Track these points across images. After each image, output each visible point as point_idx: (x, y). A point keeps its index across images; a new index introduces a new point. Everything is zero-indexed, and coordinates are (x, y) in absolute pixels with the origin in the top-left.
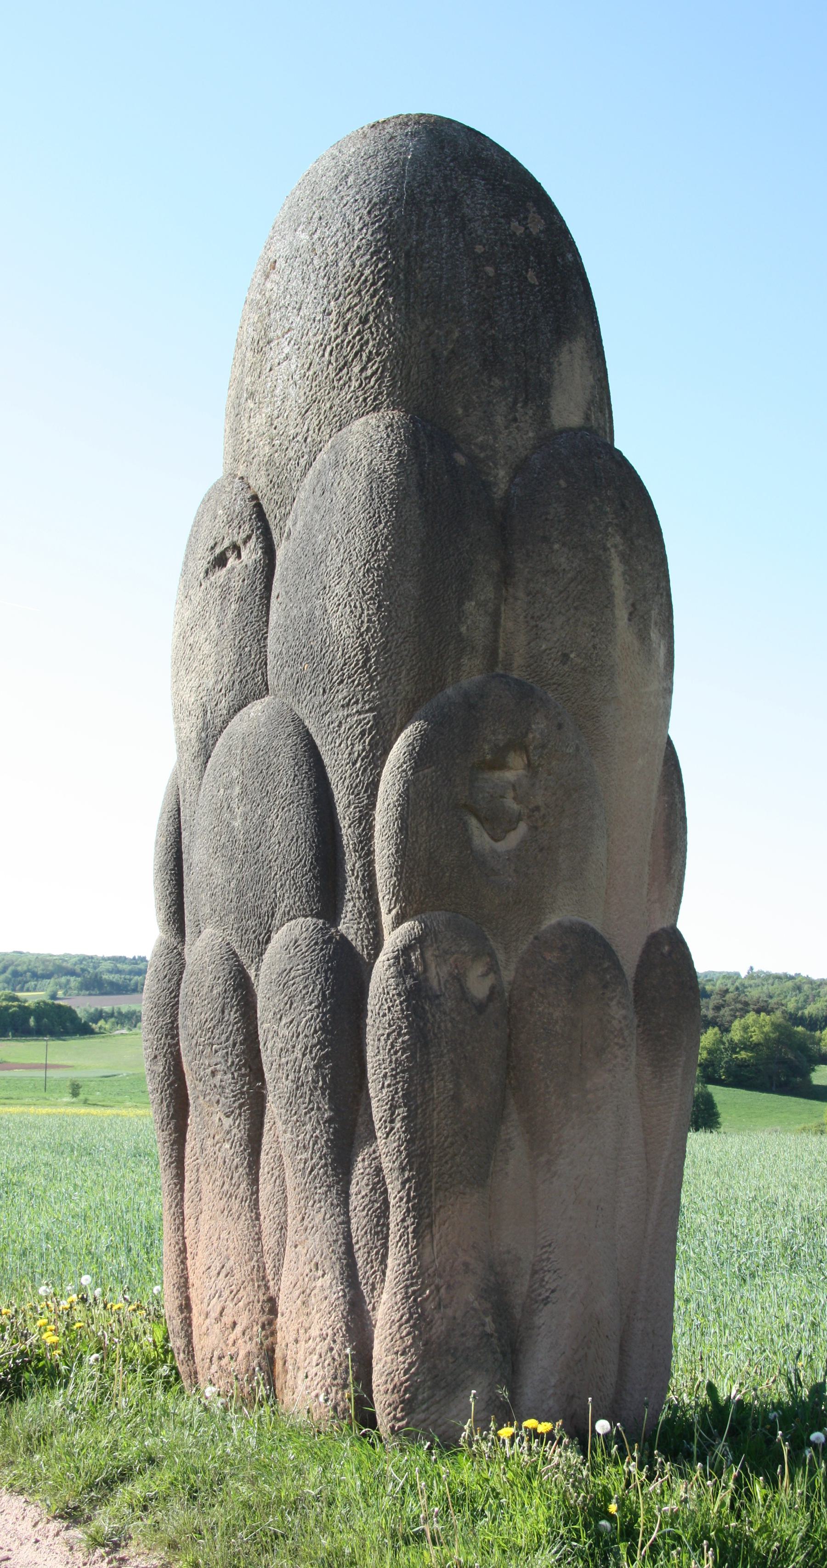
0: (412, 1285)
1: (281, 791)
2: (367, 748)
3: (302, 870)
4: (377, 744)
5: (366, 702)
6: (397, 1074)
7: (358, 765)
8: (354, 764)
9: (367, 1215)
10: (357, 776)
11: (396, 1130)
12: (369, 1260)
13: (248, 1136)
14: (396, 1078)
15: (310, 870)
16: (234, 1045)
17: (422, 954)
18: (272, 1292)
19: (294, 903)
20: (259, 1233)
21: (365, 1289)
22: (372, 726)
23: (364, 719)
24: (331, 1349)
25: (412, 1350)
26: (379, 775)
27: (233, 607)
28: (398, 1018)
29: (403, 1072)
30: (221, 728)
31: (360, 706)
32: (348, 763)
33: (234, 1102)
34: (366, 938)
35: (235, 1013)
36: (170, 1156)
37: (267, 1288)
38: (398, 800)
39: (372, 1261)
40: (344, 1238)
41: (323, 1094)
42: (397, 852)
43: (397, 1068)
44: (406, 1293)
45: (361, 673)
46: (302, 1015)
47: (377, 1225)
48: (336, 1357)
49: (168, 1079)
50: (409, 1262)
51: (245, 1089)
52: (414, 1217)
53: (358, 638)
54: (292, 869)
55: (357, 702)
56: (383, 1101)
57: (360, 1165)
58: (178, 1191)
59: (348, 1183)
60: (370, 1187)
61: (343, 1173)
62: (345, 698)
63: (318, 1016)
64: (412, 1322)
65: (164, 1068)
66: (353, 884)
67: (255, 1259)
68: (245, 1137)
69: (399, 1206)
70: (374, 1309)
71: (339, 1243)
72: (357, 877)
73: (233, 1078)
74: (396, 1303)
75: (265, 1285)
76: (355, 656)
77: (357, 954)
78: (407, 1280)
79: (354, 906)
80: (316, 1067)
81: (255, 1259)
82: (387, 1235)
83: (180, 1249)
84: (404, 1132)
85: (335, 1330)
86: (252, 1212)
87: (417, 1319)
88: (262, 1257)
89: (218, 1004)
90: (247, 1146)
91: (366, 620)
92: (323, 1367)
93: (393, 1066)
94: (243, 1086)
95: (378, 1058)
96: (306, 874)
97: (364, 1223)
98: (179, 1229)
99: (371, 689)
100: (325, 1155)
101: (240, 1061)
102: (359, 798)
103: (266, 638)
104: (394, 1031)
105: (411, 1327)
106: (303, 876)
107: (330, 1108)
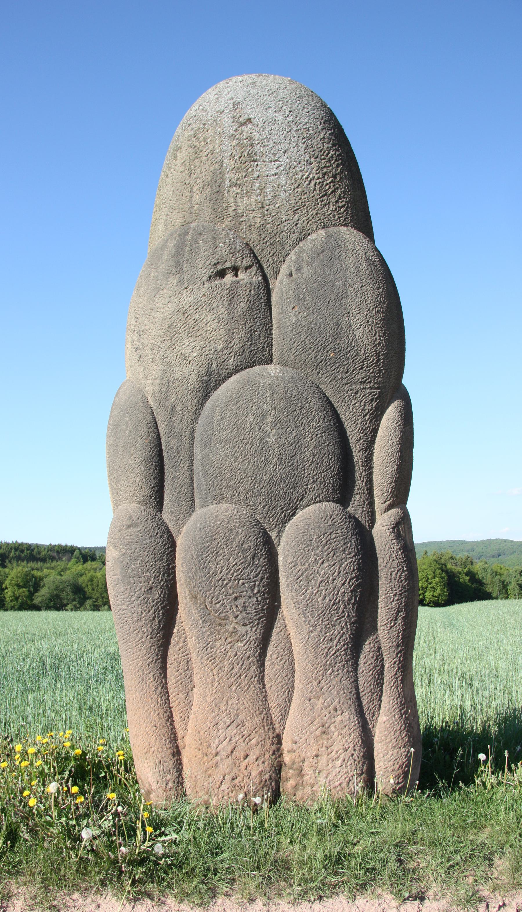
0: (403, 709)
1: (314, 424)
2: (374, 409)
3: (331, 474)
4: (378, 408)
5: (375, 383)
6: (402, 593)
7: (367, 417)
8: (364, 416)
9: (372, 674)
10: (366, 424)
11: (397, 624)
12: (372, 700)
13: (262, 637)
14: (401, 596)
15: (337, 474)
16: (262, 579)
17: (404, 527)
18: (277, 731)
19: (322, 493)
20: (266, 697)
21: (368, 717)
22: (377, 397)
23: (374, 392)
24: (353, 755)
25: (408, 744)
26: (379, 425)
27: (242, 305)
28: (402, 562)
29: (405, 592)
30: (225, 377)
31: (372, 384)
32: (360, 415)
33: (255, 616)
34: (368, 516)
35: (264, 559)
36: (157, 655)
37: (274, 729)
38: (398, 441)
39: (373, 700)
40: (356, 690)
41: (353, 607)
42: (397, 470)
43: (402, 589)
44: (401, 714)
45: (374, 366)
46: (344, 560)
47: (378, 679)
48: (356, 758)
49: (163, 603)
50: (399, 697)
51: (265, 607)
52: (401, 672)
53: (374, 347)
54: (323, 472)
55: (370, 382)
56: (392, 609)
57: (367, 647)
58: (163, 678)
59: (358, 657)
60: (375, 658)
61: (356, 653)
62: (363, 378)
63: (355, 561)
64: (406, 729)
65: (160, 596)
66: (360, 484)
67: (264, 712)
68: (260, 637)
69: (393, 667)
70: (373, 727)
71: (353, 693)
72: (363, 481)
73: (257, 601)
74: (396, 721)
75: (273, 728)
76: (372, 356)
77: (362, 525)
78: (400, 706)
79: (361, 497)
80: (352, 591)
81: (264, 712)
82: (383, 684)
83: (168, 716)
84: (402, 625)
85: (355, 743)
86: (260, 684)
87: (408, 727)
88: (269, 710)
89: (249, 554)
90: (260, 643)
91: (378, 338)
92: (347, 767)
93: (400, 589)
94: (264, 606)
95: (391, 584)
96: (334, 476)
97: (370, 679)
98: (166, 703)
99: (379, 377)
100: (347, 643)
101: (265, 589)
102: (366, 436)
103: (271, 330)
104: (400, 569)
105: (406, 731)
106: (331, 477)
107: (356, 615)
